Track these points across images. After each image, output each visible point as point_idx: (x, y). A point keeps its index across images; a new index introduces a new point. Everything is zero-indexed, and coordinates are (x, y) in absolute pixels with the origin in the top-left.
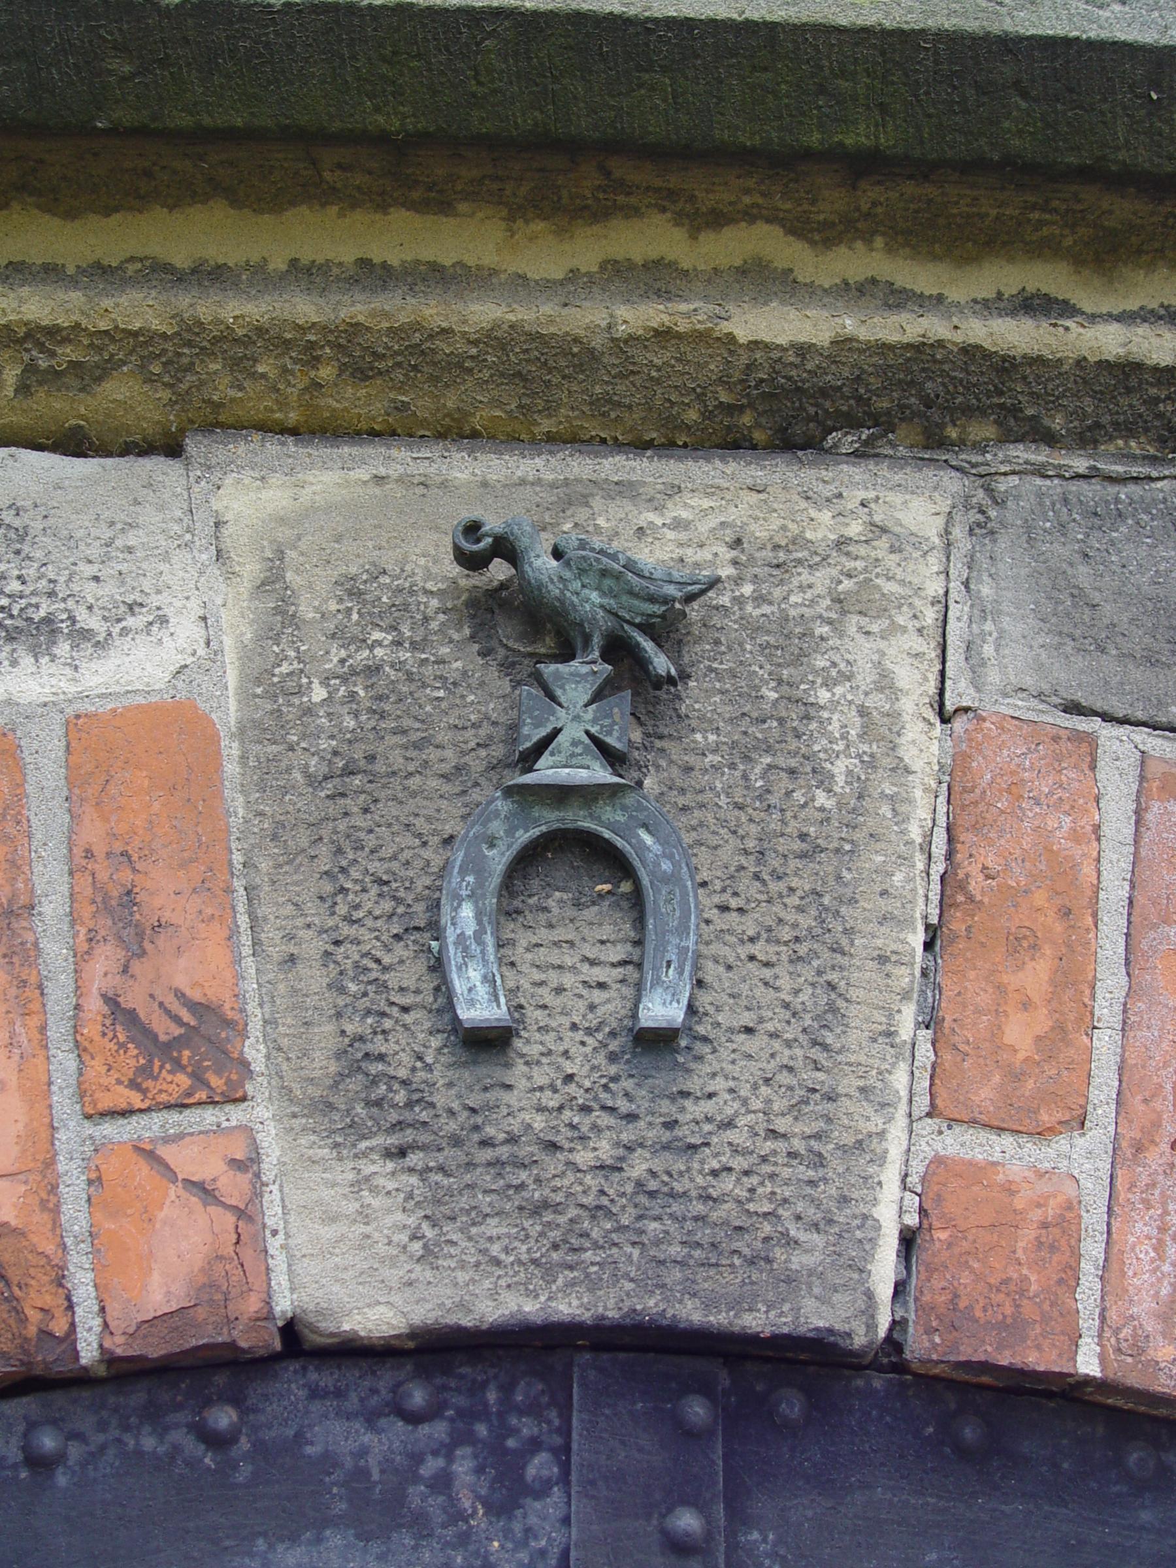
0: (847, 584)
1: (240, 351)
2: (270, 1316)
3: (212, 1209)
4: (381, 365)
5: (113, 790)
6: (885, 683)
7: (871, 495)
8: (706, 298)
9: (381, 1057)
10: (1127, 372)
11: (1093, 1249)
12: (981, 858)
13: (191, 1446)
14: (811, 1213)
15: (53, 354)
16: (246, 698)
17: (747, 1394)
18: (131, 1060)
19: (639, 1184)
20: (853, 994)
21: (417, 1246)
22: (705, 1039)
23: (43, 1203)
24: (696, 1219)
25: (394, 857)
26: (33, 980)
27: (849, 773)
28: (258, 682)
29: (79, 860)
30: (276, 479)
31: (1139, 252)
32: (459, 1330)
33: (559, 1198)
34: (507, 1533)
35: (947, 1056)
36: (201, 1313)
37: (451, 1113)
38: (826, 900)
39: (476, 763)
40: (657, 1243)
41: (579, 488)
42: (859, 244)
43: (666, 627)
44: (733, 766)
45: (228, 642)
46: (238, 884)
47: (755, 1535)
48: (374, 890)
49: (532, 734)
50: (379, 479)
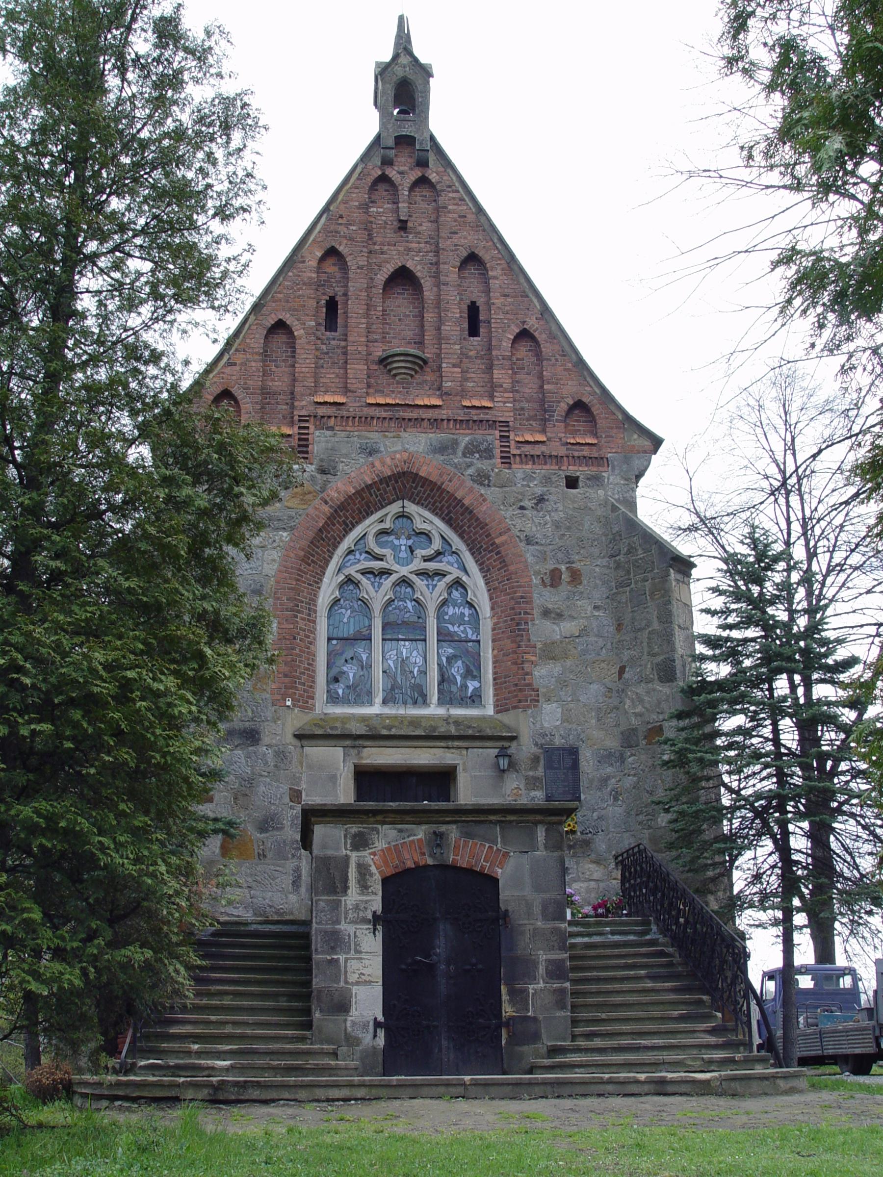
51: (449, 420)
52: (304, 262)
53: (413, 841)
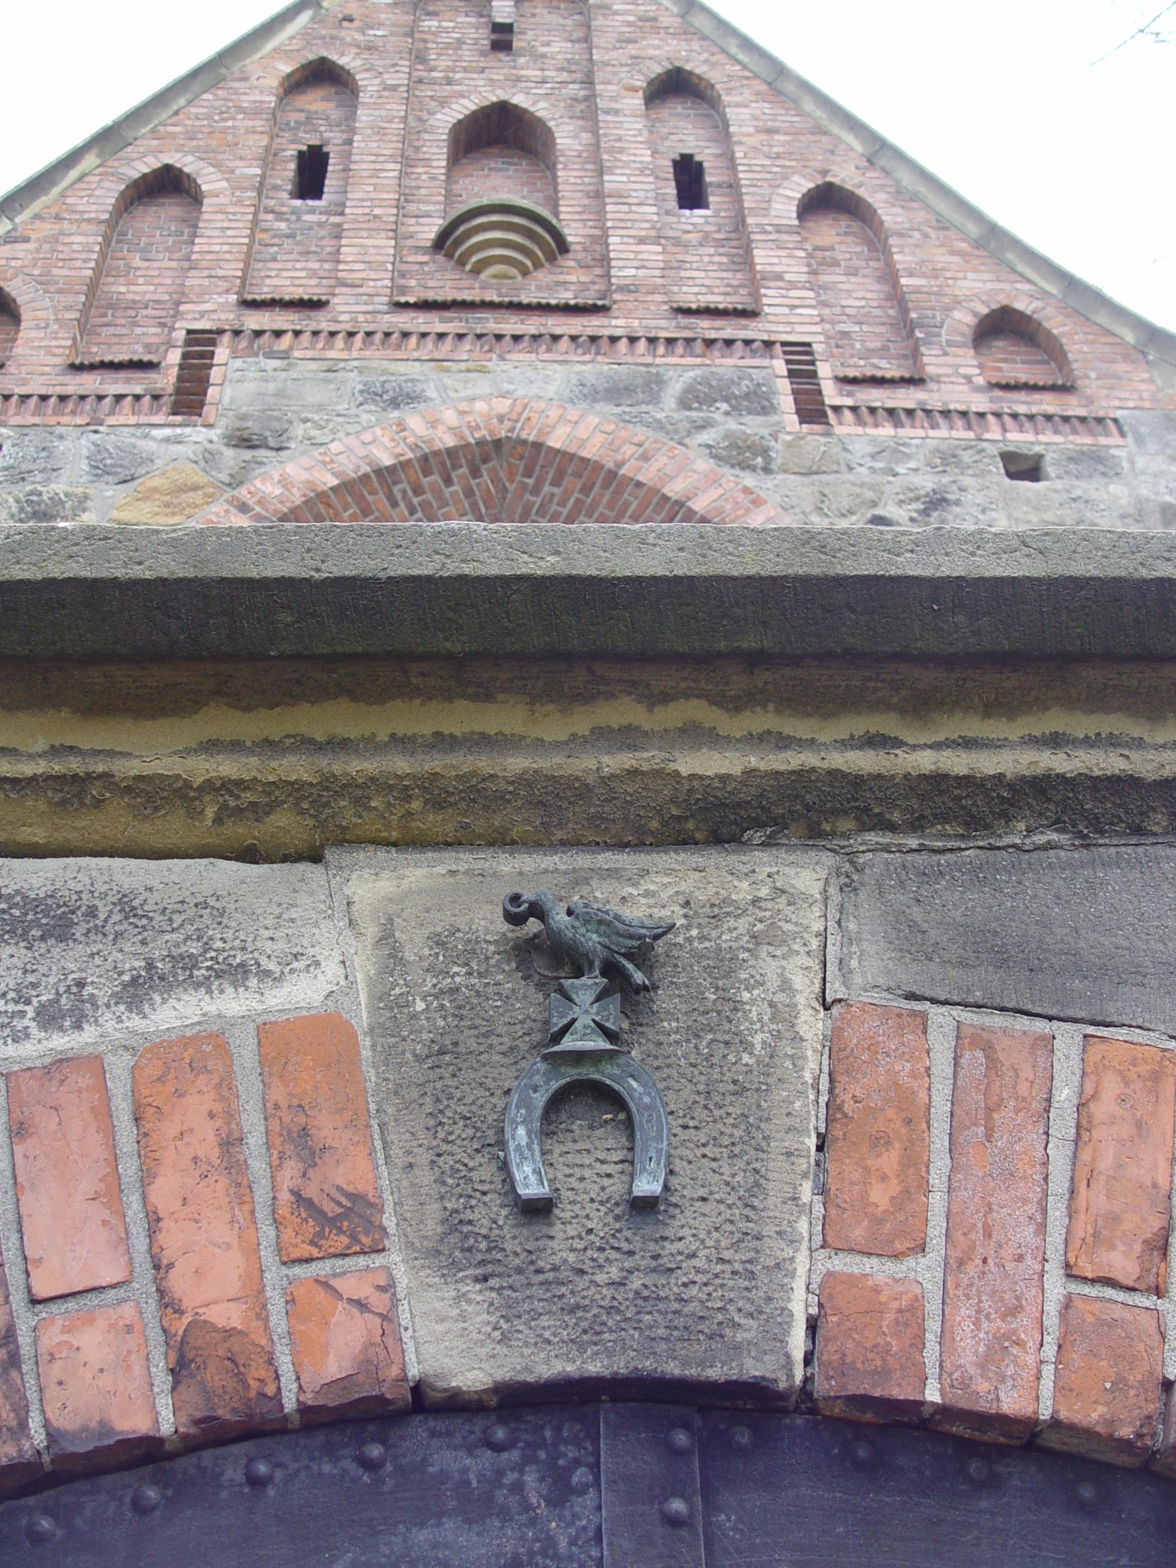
0: (759, 927)
1: (360, 792)
2: (405, 1379)
3: (366, 1315)
4: (452, 799)
5: (290, 1068)
6: (786, 986)
7: (775, 869)
8: (660, 748)
9: (470, 1222)
10: (938, 781)
11: (933, 1326)
12: (851, 1091)
13: (354, 1469)
14: (748, 1307)
15: (238, 797)
16: (373, 1010)
17: (715, 1424)
18: (311, 1228)
19: (637, 1293)
20: (771, 1175)
21: (497, 1334)
22: (676, 1205)
23: (258, 1316)
24: (674, 1312)
25: (473, 1103)
26: (245, 1183)
27: (764, 1042)
28: (380, 1000)
29: (270, 1111)
30: (385, 874)
31: (942, 703)
32: (525, 1384)
33: (587, 1302)
34: (561, 1518)
35: (833, 1211)
36: (361, 1378)
37: (516, 1254)
38: (751, 1120)
39: (523, 1045)
40: (650, 1327)
41: (583, 874)
42: (758, 709)
43: (642, 954)
44: (688, 1041)
45: (360, 976)
46: (374, 1123)
47: (723, 1517)
48: (461, 1123)
49: (559, 1023)
50: (452, 873)
51: (633, 340)
52: (246, 79)
53: (202, 1051)
